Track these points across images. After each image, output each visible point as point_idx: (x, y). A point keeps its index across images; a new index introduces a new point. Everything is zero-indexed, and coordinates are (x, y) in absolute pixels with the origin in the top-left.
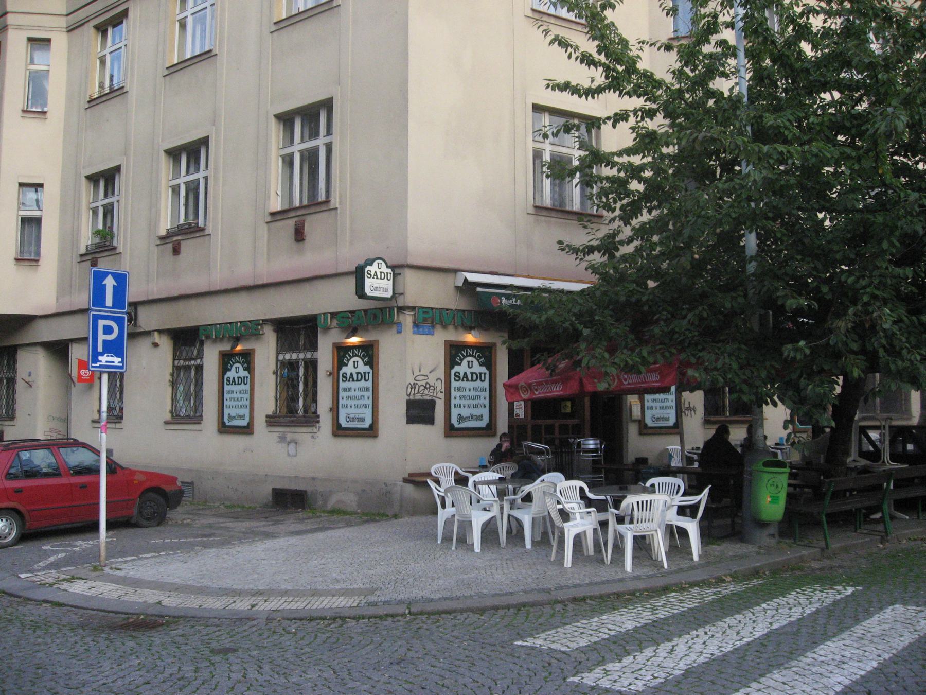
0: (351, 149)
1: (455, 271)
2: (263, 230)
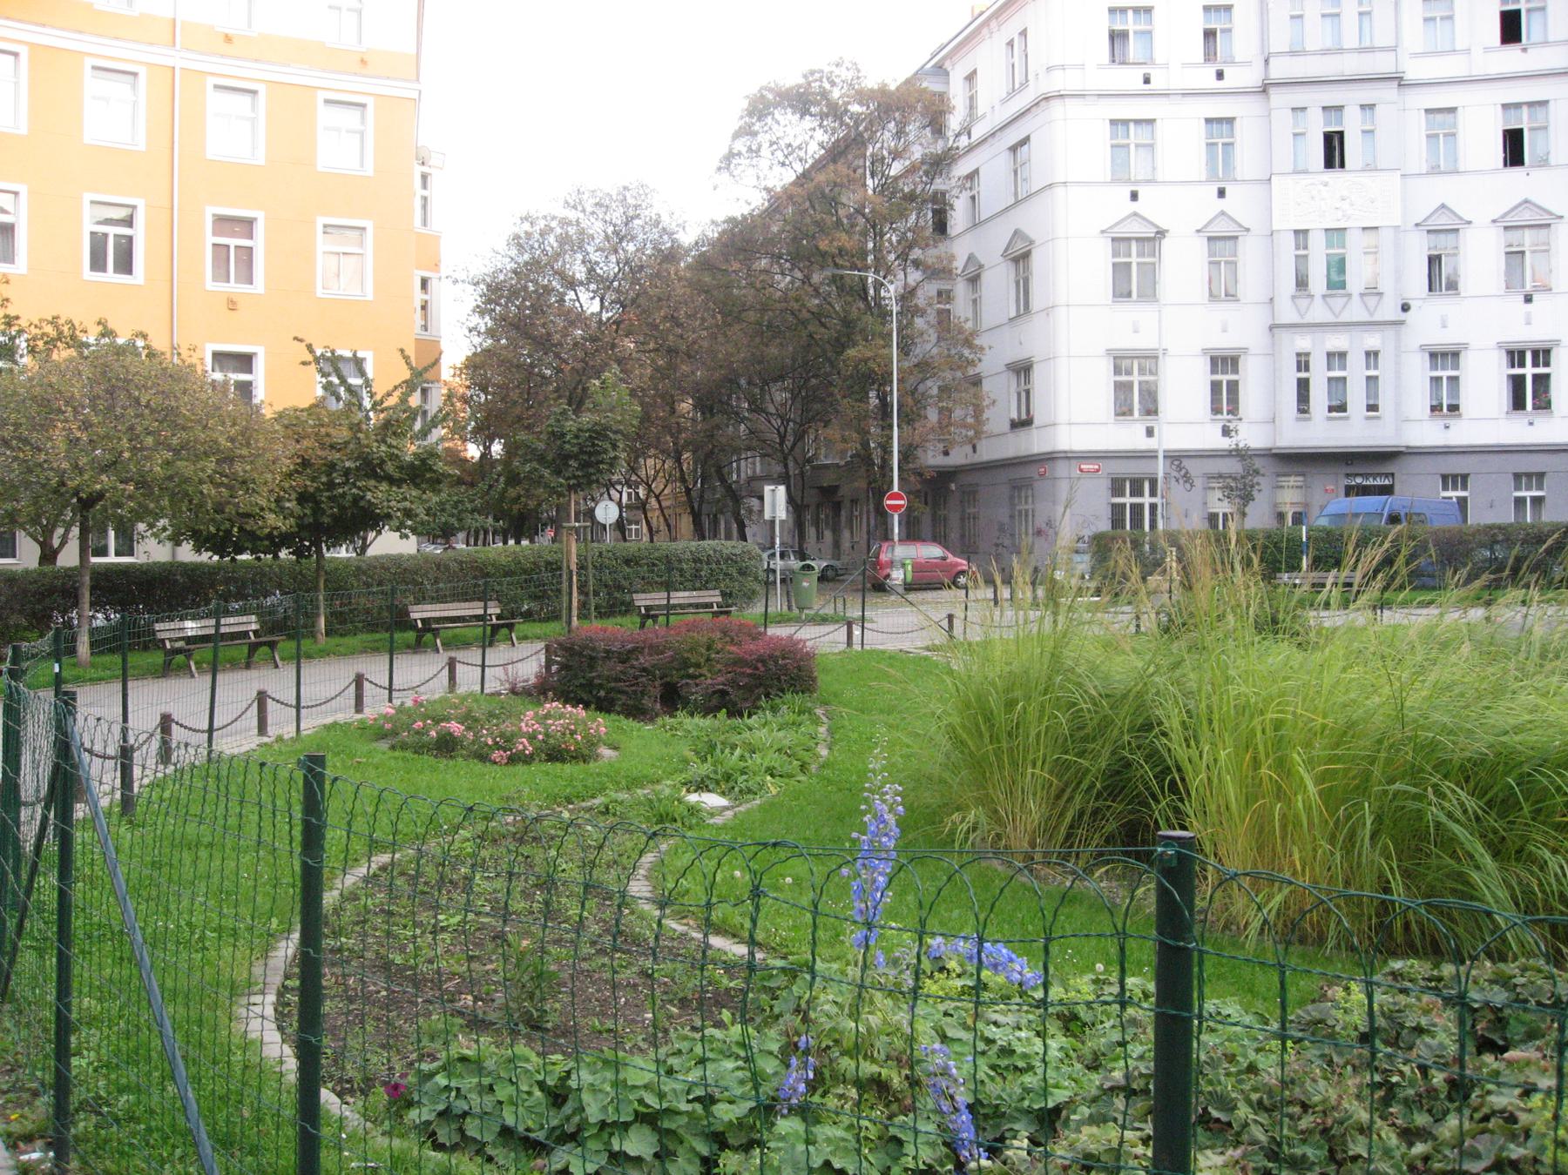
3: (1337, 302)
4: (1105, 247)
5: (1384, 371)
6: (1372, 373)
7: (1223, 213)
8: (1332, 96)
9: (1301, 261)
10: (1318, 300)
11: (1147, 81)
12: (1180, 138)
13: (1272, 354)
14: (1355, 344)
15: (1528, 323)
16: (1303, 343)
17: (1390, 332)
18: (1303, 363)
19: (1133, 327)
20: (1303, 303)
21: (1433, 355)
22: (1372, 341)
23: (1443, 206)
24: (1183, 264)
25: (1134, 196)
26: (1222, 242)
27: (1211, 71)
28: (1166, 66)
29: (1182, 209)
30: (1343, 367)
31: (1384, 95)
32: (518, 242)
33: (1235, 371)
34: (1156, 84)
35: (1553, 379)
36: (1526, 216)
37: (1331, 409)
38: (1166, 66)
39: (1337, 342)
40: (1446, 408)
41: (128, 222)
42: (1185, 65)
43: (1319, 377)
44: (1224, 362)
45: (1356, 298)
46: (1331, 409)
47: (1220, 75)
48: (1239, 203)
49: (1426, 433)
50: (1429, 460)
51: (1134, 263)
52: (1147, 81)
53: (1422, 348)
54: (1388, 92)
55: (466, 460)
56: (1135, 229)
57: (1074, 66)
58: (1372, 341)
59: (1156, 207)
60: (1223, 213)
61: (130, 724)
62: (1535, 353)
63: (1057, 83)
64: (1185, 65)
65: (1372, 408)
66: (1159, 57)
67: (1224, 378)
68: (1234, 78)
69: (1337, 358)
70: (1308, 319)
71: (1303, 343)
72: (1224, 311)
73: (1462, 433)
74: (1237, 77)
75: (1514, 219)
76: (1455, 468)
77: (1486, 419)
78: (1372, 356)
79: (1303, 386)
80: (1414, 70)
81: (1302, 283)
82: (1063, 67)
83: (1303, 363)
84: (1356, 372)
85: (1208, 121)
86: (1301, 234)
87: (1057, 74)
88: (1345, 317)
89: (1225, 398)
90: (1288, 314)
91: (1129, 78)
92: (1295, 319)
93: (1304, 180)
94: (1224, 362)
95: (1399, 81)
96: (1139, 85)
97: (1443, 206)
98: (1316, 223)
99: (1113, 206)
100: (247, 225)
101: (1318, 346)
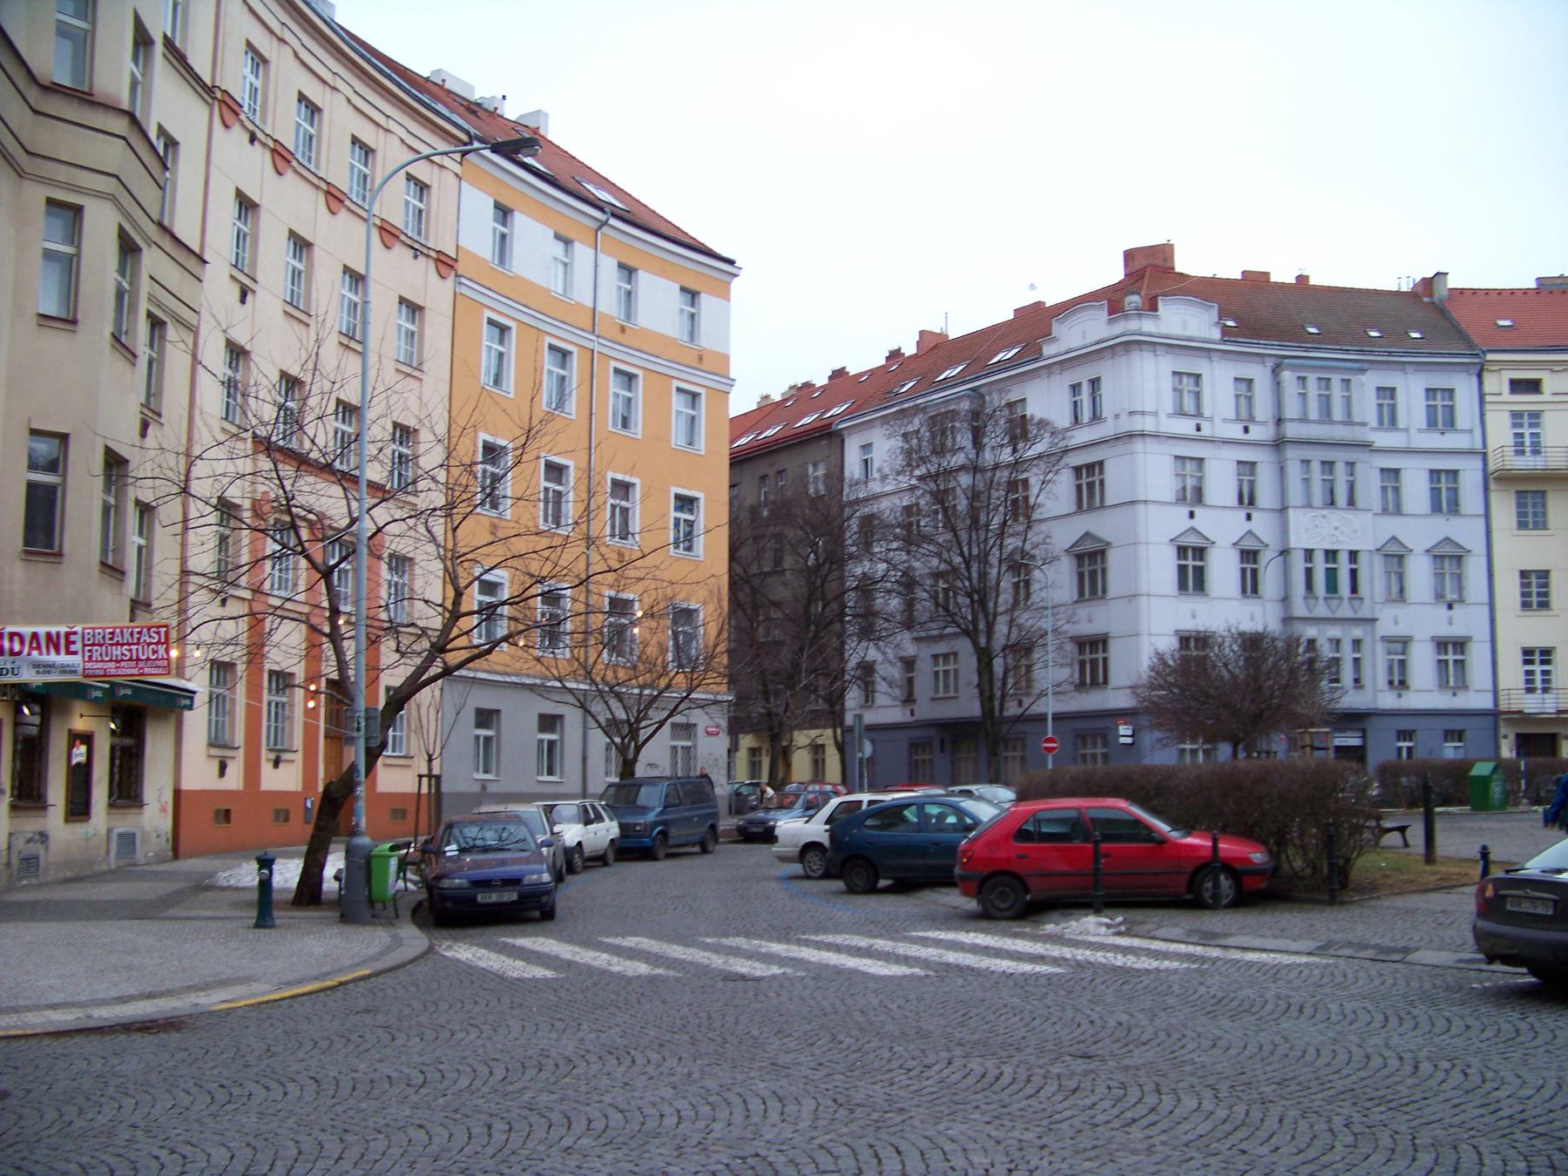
3: (1334, 603)
4: (1171, 552)
5: (1365, 653)
7: (1250, 532)
8: (1328, 455)
9: (1309, 573)
11: (1199, 429)
12: (1221, 482)
15: (1396, 623)
22: (1357, 632)
23: (1394, 538)
24: (1223, 569)
27: (1240, 427)
28: (1211, 419)
29: (1222, 527)
34: (1206, 431)
35: (1467, 663)
36: (1447, 550)
38: (1211, 419)
40: (1400, 684)
45: (1321, 601)
47: (1246, 430)
48: (1263, 526)
49: (1388, 700)
50: (1387, 720)
52: (1199, 429)
55: (747, 733)
56: (1192, 540)
57: (1150, 413)
58: (1357, 632)
59: (1206, 522)
60: (1250, 532)
61: (136, 1036)
62: (1197, 640)
63: (1139, 424)
64: (1225, 420)
66: (1207, 412)
73: (1412, 701)
75: (1438, 551)
76: (1407, 723)
77: (1424, 693)
78: (1357, 644)
82: (1143, 413)
85: (1239, 462)
86: (1309, 554)
87: (1138, 417)
88: (1339, 614)
91: (1186, 427)
92: (1307, 614)
93: (1311, 513)
96: (1191, 431)
97: (1394, 538)
98: (1320, 544)
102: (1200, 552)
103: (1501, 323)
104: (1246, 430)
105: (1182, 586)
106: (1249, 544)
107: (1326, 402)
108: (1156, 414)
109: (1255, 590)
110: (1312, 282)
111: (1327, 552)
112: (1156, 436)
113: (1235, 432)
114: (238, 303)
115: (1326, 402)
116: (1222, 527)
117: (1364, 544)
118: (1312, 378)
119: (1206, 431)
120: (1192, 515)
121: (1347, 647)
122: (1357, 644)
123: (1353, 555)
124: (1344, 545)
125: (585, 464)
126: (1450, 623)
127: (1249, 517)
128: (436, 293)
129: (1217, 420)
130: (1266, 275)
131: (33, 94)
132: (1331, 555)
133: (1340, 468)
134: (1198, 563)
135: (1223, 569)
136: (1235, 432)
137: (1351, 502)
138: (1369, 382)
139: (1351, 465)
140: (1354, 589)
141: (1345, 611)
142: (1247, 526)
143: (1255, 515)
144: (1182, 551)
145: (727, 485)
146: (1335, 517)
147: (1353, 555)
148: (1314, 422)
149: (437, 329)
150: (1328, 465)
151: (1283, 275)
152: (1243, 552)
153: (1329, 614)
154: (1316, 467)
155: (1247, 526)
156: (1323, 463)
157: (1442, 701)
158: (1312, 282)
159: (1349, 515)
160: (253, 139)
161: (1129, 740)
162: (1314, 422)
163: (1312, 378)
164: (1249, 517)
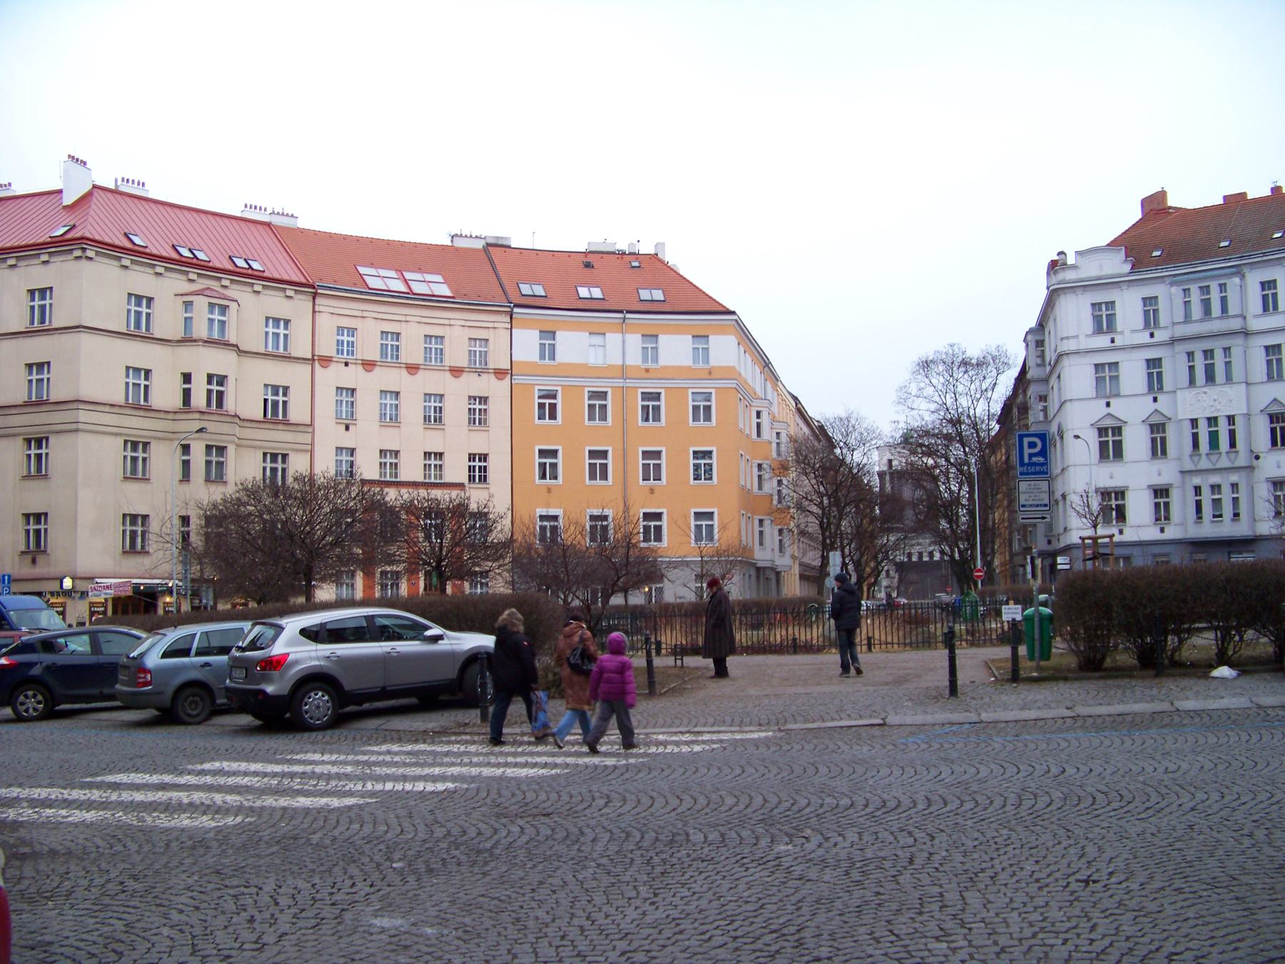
0: (56, 537)
1: (93, 578)
2: (17, 558)
5: (1242, 495)
6: (1216, 497)
8: (1207, 345)
10: (1204, 457)
11: (1113, 341)
12: (1133, 374)
13: (1183, 486)
14: (1224, 480)
15: (1279, 467)
16: (1197, 481)
17: (1243, 474)
18: (1198, 490)
19: (1110, 475)
20: (1196, 458)
21: (1156, 492)
22: (1234, 478)
24: (1136, 441)
25: (1108, 404)
26: (1157, 429)
27: (1147, 334)
28: (1122, 333)
29: (1133, 410)
30: (1220, 493)
31: (1237, 344)
32: (845, 421)
33: (1167, 496)
34: (1118, 343)
37: (1214, 516)
39: (1215, 479)
41: (554, 397)
42: (1133, 331)
43: (1206, 498)
44: (1161, 492)
45: (1224, 455)
46: (1214, 516)
47: (1152, 335)
51: (1110, 444)
52: (1113, 341)
53: (1268, 480)
54: (1239, 341)
56: (1109, 423)
58: (1234, 478)
59: (1120, 408)
62: (1116, 493)
64: (1133, 331)
65: (1236, 515)
67: (1161, 500)
68: (1157, 338)
69: (1216, 488)
70: (1199, 467)
71: (1197, 481)
72: (1159, 464)
74: (1161, 336)
78: (1235, 486)
79: (1199, 505)
80: (1255, 324)
81: (1196, 444)
82: (1067, 338)
83: (1198, 490)
84: (1226, 496)
86: (1194, 422)
88: (1218, 466)
89: (1162, 513)
90: (1189, 466)
91: (1103, 341)
92: (1193, 468)
93: (1194, 391)
94: (1161, 492)
95: (1246, 333)
98: (1201, 414)
99: (1097, 411)
100: (657, 397)
101: (1205, 482)
102: (1118, 431)
103: (1222, 244)
104: (1152, 335)
105: (1154, 453)
106: (1156, 419)
107: (1206, 304)
108: (1077, 337)
109: (1164, 452)
110: (1250, 197)
111: (1209, 419)
112: (1077, 353)
113: (1144, 338)
114: (149, 486)
115: (1206, 304)
116: (1133, 410)
117: (1238, 409)
118: (1194, 289)
119: (1118, 343)
120: (1108, 404)
121: (1226, 489)
122: (1235, 486)
123: (1231, 419)
124: (1222, 412)
125: (621, 447)
126: (1279, 467)
127: (1155, 400)
128: (498, 390)
129: (1127, 333)
130: (1243, 195)
131: (170, 416)
132: (1212, 421)
133: (1219, 355)
134: (1117, 438)
135: (1136, 441)
136: (1144, 338)
137: (1229, 378)
138: (1254, 279)
139: (1227, 350)
140: (1233, 444)
141: (1224, 462)
142: (1153, 406)
143: (1160, 397)
144: (1102, 431)
145: (1121, 378)
146: (1213, 392)
147: (1231, 419)
148: (1196, 321)
149: (498, 411)
150: (1208, 354)
151: (1258, 189)
152: (1151, 426)
153: (1210, 466)
154: (1199, 357)
155: (1153, 406)
156: (1205, 352)
157: (1152, 534)
158: (1250, 197)
159: (1227, 389)
160: (346, 364)
161: (1067, 567)
162: (1196, 321)
163: (1194, 289)
164: (1155, 400)
